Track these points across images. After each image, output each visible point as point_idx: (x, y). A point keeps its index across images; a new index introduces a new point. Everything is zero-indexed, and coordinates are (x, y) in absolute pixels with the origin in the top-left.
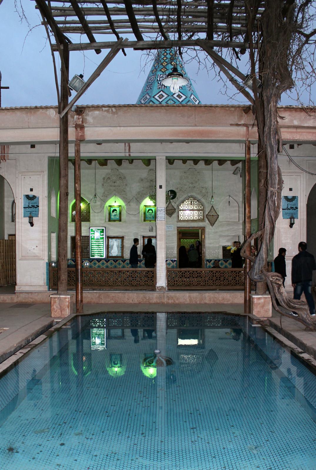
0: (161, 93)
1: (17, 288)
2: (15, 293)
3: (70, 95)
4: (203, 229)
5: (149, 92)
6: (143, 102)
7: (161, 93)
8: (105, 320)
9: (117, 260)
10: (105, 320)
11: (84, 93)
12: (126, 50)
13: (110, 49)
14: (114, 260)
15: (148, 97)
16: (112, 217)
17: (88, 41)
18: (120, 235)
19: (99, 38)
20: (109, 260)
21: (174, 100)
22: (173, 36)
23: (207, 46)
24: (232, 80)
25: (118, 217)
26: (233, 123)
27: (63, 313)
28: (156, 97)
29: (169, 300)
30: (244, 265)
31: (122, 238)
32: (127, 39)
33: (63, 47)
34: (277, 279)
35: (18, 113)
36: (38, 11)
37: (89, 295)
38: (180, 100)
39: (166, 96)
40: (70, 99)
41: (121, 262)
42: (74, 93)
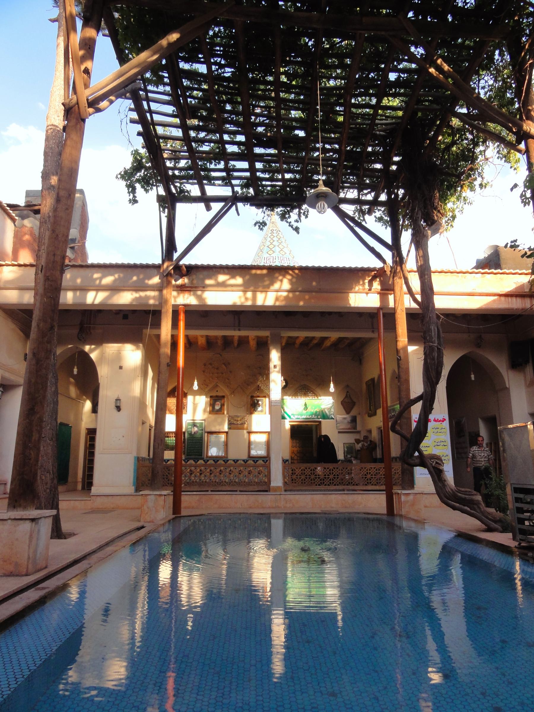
2: (90, 497)
3: (176, 251)
29: (286, 503)
30: (473, 379)
34: (437, 463)
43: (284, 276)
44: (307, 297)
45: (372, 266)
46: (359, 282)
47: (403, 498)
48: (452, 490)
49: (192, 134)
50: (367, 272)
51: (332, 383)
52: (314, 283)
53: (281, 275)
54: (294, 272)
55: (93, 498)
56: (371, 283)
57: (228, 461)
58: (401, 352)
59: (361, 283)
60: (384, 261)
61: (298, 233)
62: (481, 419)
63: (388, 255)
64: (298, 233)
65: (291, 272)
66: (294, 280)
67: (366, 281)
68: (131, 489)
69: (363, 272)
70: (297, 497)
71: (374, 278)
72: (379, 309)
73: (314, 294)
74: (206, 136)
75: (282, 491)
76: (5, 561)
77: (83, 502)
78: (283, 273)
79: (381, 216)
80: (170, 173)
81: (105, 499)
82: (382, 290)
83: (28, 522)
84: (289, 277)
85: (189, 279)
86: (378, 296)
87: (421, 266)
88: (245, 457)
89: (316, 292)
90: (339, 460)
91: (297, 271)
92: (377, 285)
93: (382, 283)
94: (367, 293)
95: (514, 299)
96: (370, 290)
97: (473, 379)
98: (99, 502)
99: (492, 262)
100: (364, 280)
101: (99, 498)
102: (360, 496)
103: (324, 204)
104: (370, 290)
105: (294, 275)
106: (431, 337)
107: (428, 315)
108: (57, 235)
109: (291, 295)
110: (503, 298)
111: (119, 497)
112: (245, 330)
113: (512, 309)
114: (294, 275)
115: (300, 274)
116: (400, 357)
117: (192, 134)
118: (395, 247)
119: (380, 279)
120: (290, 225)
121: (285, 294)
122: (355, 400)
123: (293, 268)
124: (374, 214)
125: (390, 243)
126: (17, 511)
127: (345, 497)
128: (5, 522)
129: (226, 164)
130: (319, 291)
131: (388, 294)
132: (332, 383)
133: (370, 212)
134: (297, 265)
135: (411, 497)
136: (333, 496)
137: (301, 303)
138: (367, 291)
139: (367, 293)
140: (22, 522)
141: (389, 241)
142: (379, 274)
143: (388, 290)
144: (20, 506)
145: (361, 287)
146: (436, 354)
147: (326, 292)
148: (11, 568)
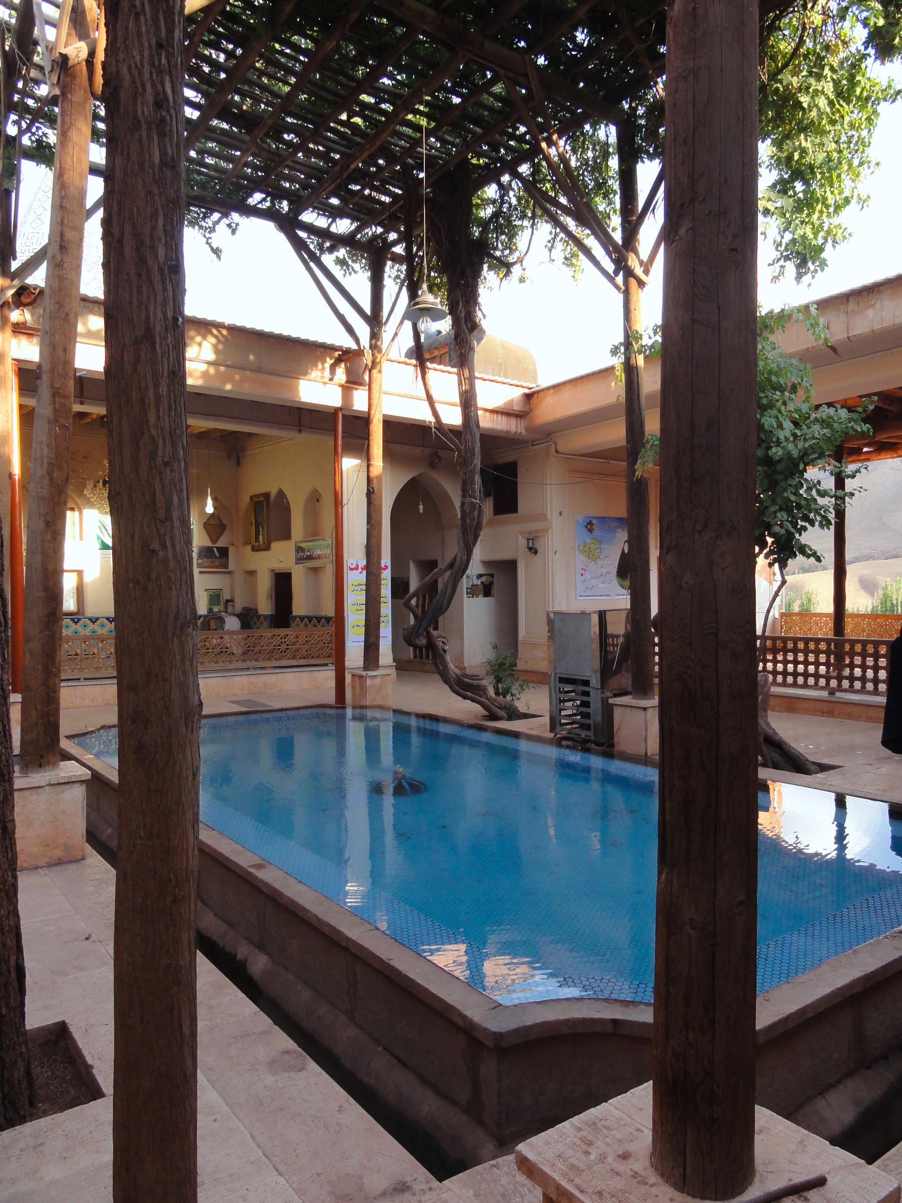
3: (15, 258)
30: (421, 511)
43: (204, 338)
44: (237, 377)
45: (337, 343)
46: (317, 366)
47: (369, 682)
48: (456, 675)
50: (329, 351)
51: (209, 498)
52: (252, 357)
53: (199, 334)
54: (220, 332)
56: (333, 367)
58: (375, 481)
59: (320, 367)
60: (357, 341)
61: (219, 257)
62: (414, 562)
63: (363, 330)
64: (219, 257)
65: (215, 332)
66: (221, 347)
67: (327, 366)
69: (322, 350)
71: (338, 361)
72: (337, 410)
73: (248, 373)
74: (358, 230)
76: (48, 845)
78: (203, 331)
79: (344, 258)
80: (16, 98)
82: (347, 382)
83: (77, 785)
84: (213, 340)
85: (32, 315)
86: (339, 390)
87: (466, 392)
89: (252, 370)
90: (200, 617)
91: (225, 332)
92: (341, 374)
93: (348, 372)
94: (325, 383)
95: (500, 417)
96: (331, 379)
97: (421, 511)
100: (324, 362)
102: (274, 677)
104: (331, 379)
105: (221, 338)
106: (474, 490)
107: (472, 461)
108: (67, 314)
109: (212, 370)
110: (488, 414)
112: (92, 404)
113: (496, 430)
114: (221, 338)
115: (229, 337)
116: (373, 488)
118: (375, 320)
119: (346, 366)
120: (207, 243)
121: (204, 367)
122: (225, 522)
123: (218, 326)
124: (336, 254)
125: (369, 314)
126: (45, 772)
127: (254, 679)
128: (40, 790)
130: (259, 370)
131: (352, 389)
132: (209, 498)
133: (331, 250)
134: (228, 321)
135: (378, 680)
136: (237, 679)
137: (228, 387)
138: (326, 380)
139: (325, 383)
140: (68, 786)
141: (368, 310)
142: (346, 356)
143: (355, 383)
144: (48, 763)
145: (319, 374)
146: (476, 513)
147: (269, 373)
148: (58, 853)
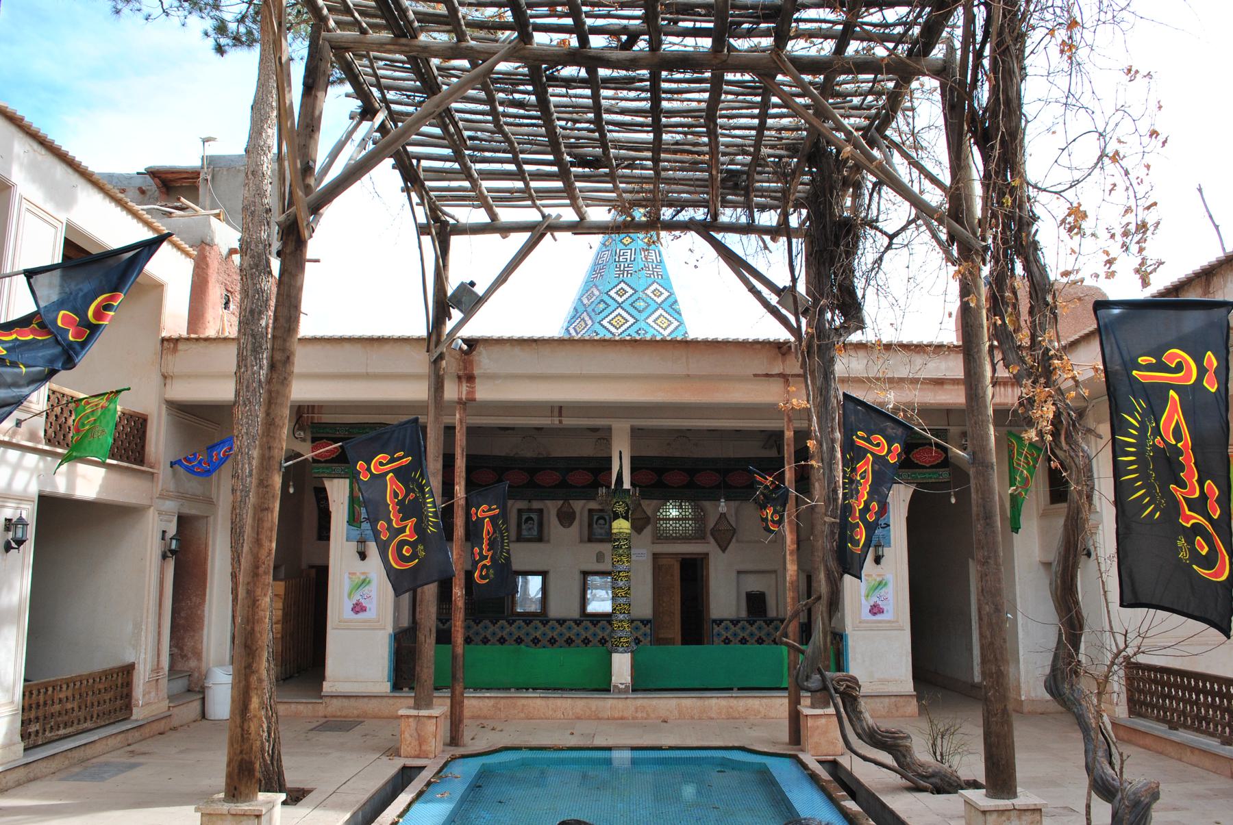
0: (622, 285)
1: (327, 687)
2: (321, 697)
3: (450, 318)
4: (707, 554)
5: (597, 282)
6: (585, 301)
7: (622, 285)
8: (953, 501)
9: (531, 621)
10: (953, 501)
11: (366, 178)
12: (556, 234)
13: (529, 234)
14: (591, 622)
15: (597, 293)
16: (525, 533)
17: (488, 220)
18: (578, 577)
19: (506, 215)
20: (514, 621)
21: (648, 300)
22: (639, 214)
23: (706, 229)
24: (752, 290)
25: (535, 533)
26: (759, 372)
27: (424, 748)
28: (612, 293)
31: (585, 574)
32: (559, 216)
33: (440, 231)
34: (848, 686)
35: (347, 346)
36: (397, 172)
37: (474, 702)
38: (655, 286)
39: (631, 292)
40: (449, 325)
41: (540, 625)
42: (456, 315)
49: (501, 109)
55: (327, 700)
57: (548, 621)
68: (386, 687)
70: (654, 702)
75: (39, 442)
77: (310, 706)
81: (346, 702)
88: (576, 614)
98: (334, 706)
99: (363, 556)
101: (334, 701)
103: (722, 109)
111: (366, 700)
117: (501, 109)
127: (733, 702)
129: (584, 41)
136: (714, 701)
